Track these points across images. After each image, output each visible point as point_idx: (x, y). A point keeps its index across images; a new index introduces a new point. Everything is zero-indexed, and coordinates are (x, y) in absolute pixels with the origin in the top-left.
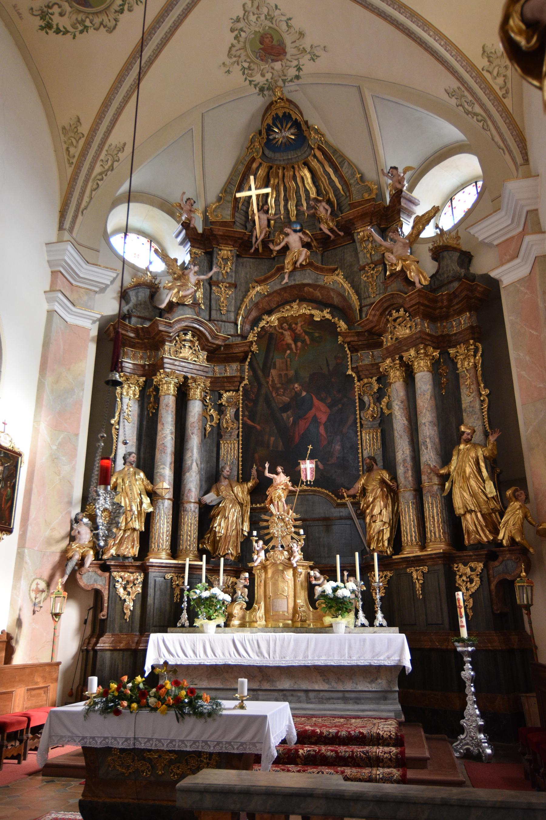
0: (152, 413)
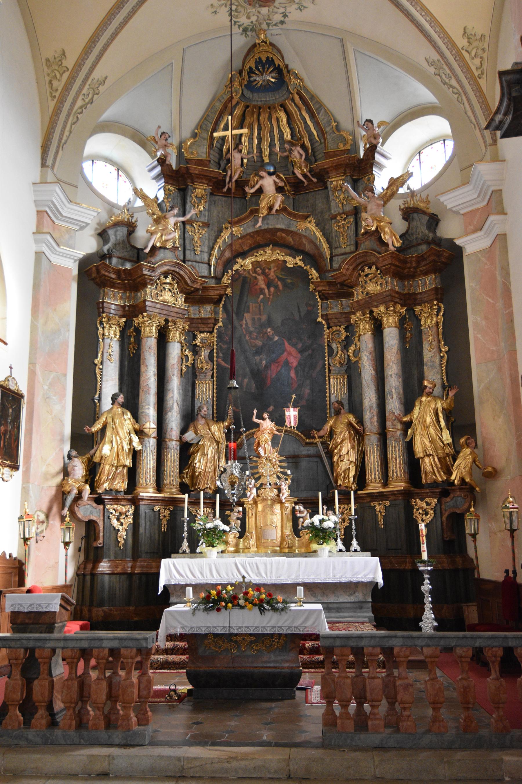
0: (133, 353)
